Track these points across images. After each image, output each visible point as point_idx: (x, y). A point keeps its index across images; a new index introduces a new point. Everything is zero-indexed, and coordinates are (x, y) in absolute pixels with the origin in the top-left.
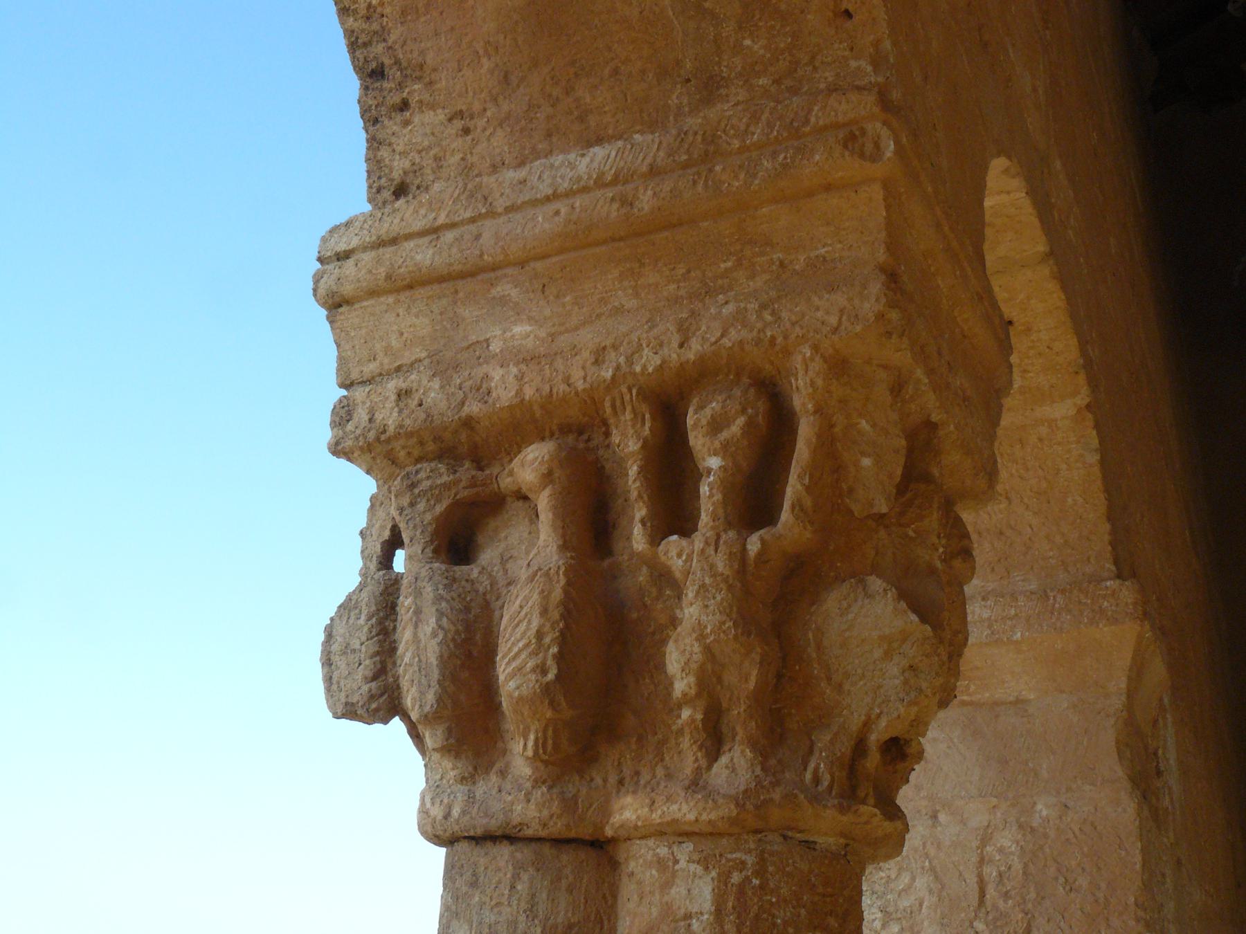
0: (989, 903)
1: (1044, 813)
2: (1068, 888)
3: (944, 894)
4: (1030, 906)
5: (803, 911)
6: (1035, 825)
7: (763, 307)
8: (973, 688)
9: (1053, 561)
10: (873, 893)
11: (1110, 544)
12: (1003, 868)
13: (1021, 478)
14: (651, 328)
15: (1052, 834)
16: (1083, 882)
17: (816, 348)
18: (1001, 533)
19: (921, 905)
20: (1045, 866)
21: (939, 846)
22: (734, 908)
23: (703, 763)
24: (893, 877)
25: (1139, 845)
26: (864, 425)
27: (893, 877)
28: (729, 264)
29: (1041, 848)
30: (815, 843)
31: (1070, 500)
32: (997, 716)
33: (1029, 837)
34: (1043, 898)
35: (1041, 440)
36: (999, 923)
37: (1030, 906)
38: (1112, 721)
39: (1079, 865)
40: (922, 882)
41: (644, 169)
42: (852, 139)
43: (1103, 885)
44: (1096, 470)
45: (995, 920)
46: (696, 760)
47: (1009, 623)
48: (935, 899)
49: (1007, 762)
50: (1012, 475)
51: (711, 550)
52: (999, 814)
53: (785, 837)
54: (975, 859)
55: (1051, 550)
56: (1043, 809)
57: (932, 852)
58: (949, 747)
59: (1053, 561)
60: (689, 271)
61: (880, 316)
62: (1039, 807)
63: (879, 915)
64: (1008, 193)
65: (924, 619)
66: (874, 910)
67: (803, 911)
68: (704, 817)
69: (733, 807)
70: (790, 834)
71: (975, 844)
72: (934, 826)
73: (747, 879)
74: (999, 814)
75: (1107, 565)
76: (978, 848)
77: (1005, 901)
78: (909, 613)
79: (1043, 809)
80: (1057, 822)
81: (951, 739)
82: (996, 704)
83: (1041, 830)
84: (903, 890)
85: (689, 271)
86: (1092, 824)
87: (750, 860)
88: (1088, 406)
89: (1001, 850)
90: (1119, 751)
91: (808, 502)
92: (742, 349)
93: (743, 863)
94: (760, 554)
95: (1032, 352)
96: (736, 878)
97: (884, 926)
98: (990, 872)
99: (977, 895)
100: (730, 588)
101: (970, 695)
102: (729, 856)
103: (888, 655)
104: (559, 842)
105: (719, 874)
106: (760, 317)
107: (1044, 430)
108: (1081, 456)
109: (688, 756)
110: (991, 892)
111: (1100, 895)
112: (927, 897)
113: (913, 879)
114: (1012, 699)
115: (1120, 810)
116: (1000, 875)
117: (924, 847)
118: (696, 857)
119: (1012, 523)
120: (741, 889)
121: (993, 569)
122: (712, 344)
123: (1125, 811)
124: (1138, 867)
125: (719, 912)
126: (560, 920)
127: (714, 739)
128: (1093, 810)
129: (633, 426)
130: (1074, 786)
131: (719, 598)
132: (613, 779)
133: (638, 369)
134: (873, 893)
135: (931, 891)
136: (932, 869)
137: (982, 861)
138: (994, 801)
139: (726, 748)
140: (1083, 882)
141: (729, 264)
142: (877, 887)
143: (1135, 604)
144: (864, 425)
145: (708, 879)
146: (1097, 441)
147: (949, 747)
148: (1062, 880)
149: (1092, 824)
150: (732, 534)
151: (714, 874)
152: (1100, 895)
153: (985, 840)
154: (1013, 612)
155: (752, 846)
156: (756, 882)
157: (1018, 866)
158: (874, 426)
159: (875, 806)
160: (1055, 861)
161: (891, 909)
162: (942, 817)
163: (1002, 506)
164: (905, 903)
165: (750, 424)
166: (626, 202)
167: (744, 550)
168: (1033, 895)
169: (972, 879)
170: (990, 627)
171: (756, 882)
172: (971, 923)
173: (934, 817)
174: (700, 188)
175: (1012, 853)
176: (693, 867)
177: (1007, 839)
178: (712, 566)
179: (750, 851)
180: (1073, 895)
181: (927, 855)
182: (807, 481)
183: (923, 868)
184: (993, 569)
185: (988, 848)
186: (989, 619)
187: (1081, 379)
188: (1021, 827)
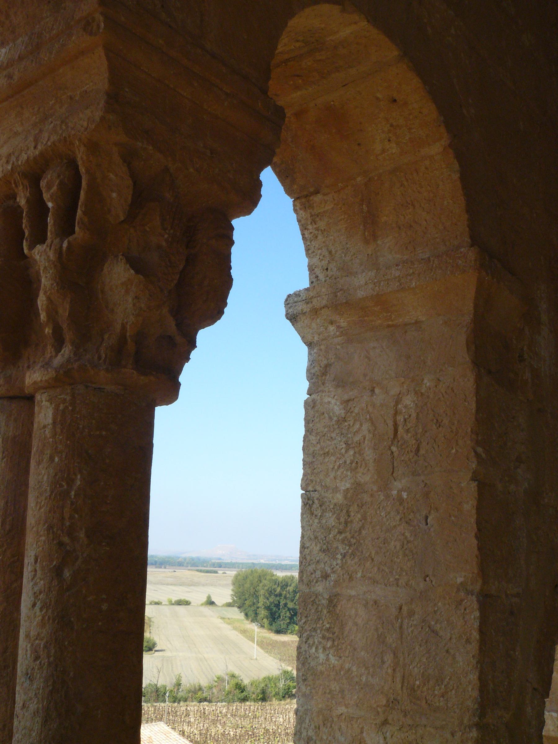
0: (399, 436)
1: (428, 384)
2: (438, 425)
3: (376, 432)
4: (419, 436)
5: (94, 421)
6: (423, 391)
7: (62, 122)
8: (393, 316)
9: (438, 240)
10: (342, 434)
11: (468, 226)
12: (406, 417)
13: (419, 192)
14: (25, 141)
15: (431, 396)
16: (446, 421)
17: (80, 140)
18: (411, 226)
19: (364, 439)
20: (428, 414)
21: (374, 406)
22: (60, 421)
23: (54, 353)
24: (351, 425)
25: (475, 398)
26: (112, 176)
27: (351, 425)
28: (53, 102)
29: (426, 404)
30: (104, 389)
31: (445, 202)
32: (406, 332)
33: (420, 398)
34: (426, 432)
35: (426, 168)
36: (403, 447)
37: (419, 436)
38: (465, 329)
39: (444, 412)
40: (366, 426)
41: (17, 58)
42: (87, 25)
43: (456, 422)
44: (458, 183)
45: (402, 445)
46: (51, 352)
47: (409, 278)
48: (371, 435)
49: (410, 357)
50: (414, 191)
51: (48, 249)
52: (405, 387)
53: (87, 387)
54: (392, 412)
55: (437, 233)
56: (427, 383)
57: (370, 409)
58: (381, 351)
59: (438, 240)
60: (39, 109)
61: (102, 119)
62: (425, 381)
63: (344, 446)
64: (356, 23)
65: (137, 272)
66: (342, 443)
67: (94, 421)
68: (44, 379)
69: (54, 372)
70: (89, 384)
71: (392, 404)
72: (372, 396)
73: (66, 407)
74: (405, 387)
75: (466, 239)
76: (394, 406)
77: (407, 435)
78: (131, 270)
79: (427, 383)
80: (434, 389)
81: (382, 347)
82: (406, 325)
83: (426, 394)
84: (356, 432)
85: (39, 109)
86: (452, 389)
87: (68, 398)
88: (450, 146)
89: (406, 407)
90: (468, 346)
91: (86, 220)
92: (55, 145)
93: (65, 399)
94: (68, 247)
95: (411, 117)
96: (62, 407)
97: (346, 452)
98: (400, 418)
99: (393, 432)
100: (55, 266)
101: (392, 321)
102: (59, 397)
103: (127, 292)
104: (11, 398)
105: (55, 406)
106: (61, 128)
107: (427, 163)
108: (450, 175)
109: (50, 350)
110: (400, 430)
111: (454, 428)
112: (367, 435)
113: (361, 425)
114: (413, 321)
115: (466, 379)
116: (405, 420)
117: (367, 407)
118: (47, 399)
119: (417, 220)
120: (63, 411)
121: (407, 248)
122: (45, 145)
123: (469, 380)
124: (474, 411)
125: (54, 423)
126: (10, 434)
127: (59, 343)
128: (452, 381)
129: (23, 192)
130: (444, 368)
131: (51, 272)
132: (26, 365)
133: (20, 163)
134: (342, 434)
135: (369, 431)
136: (371, 419)
137: (396, 413)
138: (403, 380)
139: (64, 346)
140: (446, 421)
141: (53, 102)
142: (344, 431)
143: (475, 260)
144: (112, 176)
145: (51, 408)
146: (458, 165)
147: (381, 351)
148: (435, 421)
149: (452, 389)
150: (58, 240)
151: (53, 406)
152: (454, 428)
153: (398, 401)
154: (411, 271)
155: (69, 391)
156: (70, 408)
157: (414, 415)
158: (116, 175)
159: (132, 369)
160: (433, 411)
161: (349, 442)
162: (377, 391)
163: (410, 210)
164: (357, 438)
165: (61, 183)
166: (10, 77)
167: (61, 247)
168: (421, 430)
169: (391, 423)
170: (399, 281)
171: (70, 408)
172: (390, 447)
173: (373, 391)
174: (34, 65)
175: (411, 408)
176: (47, 403)
177: (408, 401)
178: (48, 257)
179: (67, 394)
180: (440, 429)
181: (368, 412)
182: (83, 209)
183: (366, 419)
184: (407, 248)
185: (399, 406)
186: (399, 276)
187: (442, 129)
188: (416, 393)
